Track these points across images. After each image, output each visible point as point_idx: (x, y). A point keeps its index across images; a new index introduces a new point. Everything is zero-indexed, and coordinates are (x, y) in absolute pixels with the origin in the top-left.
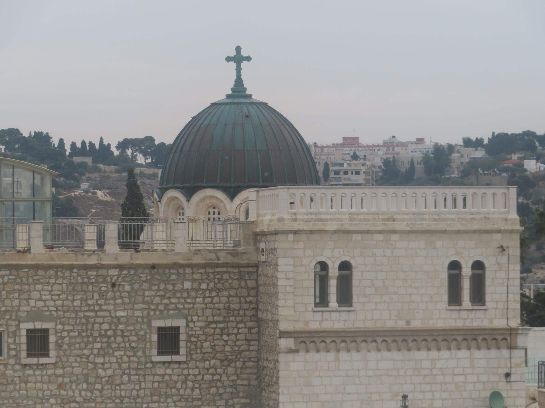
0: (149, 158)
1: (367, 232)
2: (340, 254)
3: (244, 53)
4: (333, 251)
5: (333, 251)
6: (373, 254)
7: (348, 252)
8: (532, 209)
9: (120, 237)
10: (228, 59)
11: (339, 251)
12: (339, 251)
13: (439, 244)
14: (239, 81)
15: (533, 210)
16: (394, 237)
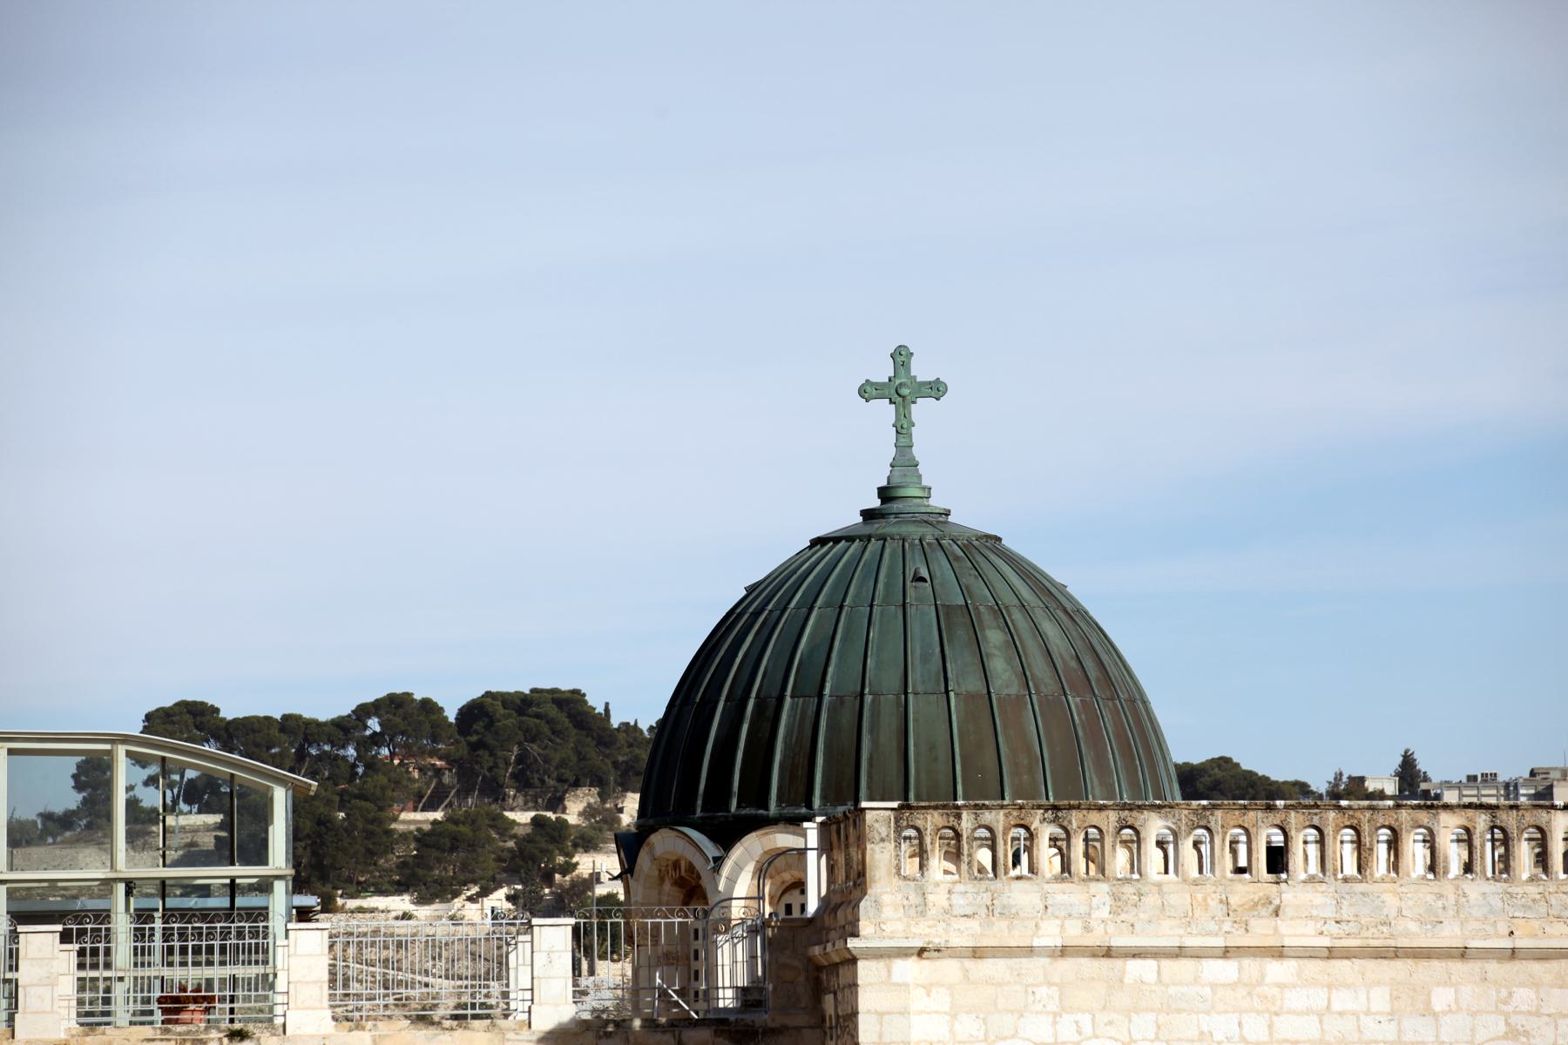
0: (1201, 783)
1: (1179, 953)
2: (1080, 1033)
3: (921, 370)
4: (1055, 1023)
5: (1055, 1023)
6: (1202, 1033)
7: (1110, 1023)
8: (855, 935)
9: (336, 979)
10: (868, 391)
11: (1077, 1022)
12: (1077, 1022)
13: (1442, 998)
14: (904, 460)
15: (991, 645)
16: (1277, 970)
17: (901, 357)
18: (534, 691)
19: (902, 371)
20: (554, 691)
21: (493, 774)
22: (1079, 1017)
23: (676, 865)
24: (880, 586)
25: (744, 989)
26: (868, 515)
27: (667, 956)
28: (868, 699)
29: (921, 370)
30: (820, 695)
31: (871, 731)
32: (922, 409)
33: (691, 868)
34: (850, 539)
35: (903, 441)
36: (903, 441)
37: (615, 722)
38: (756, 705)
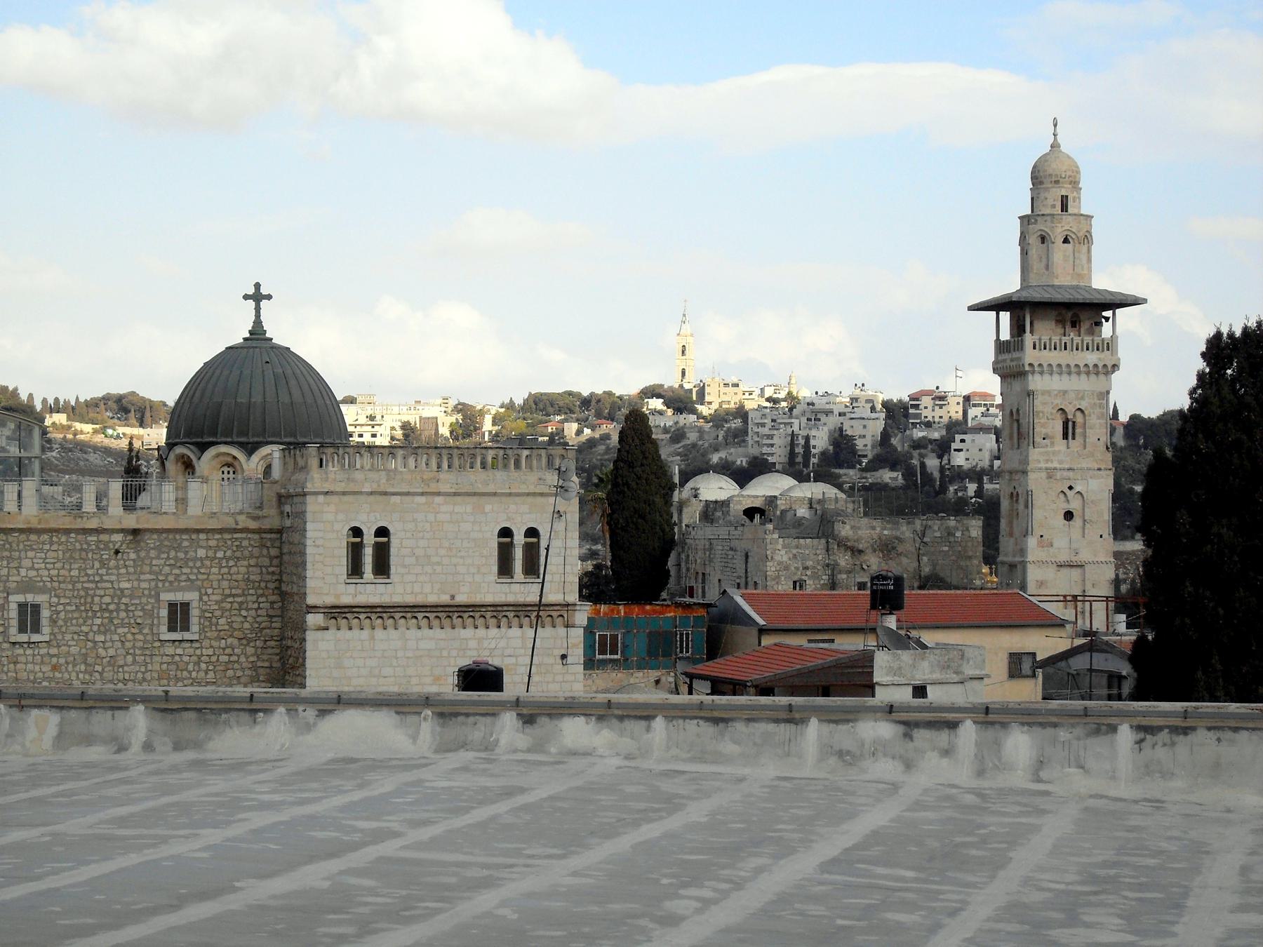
10: (246, 297)
14: (258, 322)
26: (245, 339)
32: (264, 303)
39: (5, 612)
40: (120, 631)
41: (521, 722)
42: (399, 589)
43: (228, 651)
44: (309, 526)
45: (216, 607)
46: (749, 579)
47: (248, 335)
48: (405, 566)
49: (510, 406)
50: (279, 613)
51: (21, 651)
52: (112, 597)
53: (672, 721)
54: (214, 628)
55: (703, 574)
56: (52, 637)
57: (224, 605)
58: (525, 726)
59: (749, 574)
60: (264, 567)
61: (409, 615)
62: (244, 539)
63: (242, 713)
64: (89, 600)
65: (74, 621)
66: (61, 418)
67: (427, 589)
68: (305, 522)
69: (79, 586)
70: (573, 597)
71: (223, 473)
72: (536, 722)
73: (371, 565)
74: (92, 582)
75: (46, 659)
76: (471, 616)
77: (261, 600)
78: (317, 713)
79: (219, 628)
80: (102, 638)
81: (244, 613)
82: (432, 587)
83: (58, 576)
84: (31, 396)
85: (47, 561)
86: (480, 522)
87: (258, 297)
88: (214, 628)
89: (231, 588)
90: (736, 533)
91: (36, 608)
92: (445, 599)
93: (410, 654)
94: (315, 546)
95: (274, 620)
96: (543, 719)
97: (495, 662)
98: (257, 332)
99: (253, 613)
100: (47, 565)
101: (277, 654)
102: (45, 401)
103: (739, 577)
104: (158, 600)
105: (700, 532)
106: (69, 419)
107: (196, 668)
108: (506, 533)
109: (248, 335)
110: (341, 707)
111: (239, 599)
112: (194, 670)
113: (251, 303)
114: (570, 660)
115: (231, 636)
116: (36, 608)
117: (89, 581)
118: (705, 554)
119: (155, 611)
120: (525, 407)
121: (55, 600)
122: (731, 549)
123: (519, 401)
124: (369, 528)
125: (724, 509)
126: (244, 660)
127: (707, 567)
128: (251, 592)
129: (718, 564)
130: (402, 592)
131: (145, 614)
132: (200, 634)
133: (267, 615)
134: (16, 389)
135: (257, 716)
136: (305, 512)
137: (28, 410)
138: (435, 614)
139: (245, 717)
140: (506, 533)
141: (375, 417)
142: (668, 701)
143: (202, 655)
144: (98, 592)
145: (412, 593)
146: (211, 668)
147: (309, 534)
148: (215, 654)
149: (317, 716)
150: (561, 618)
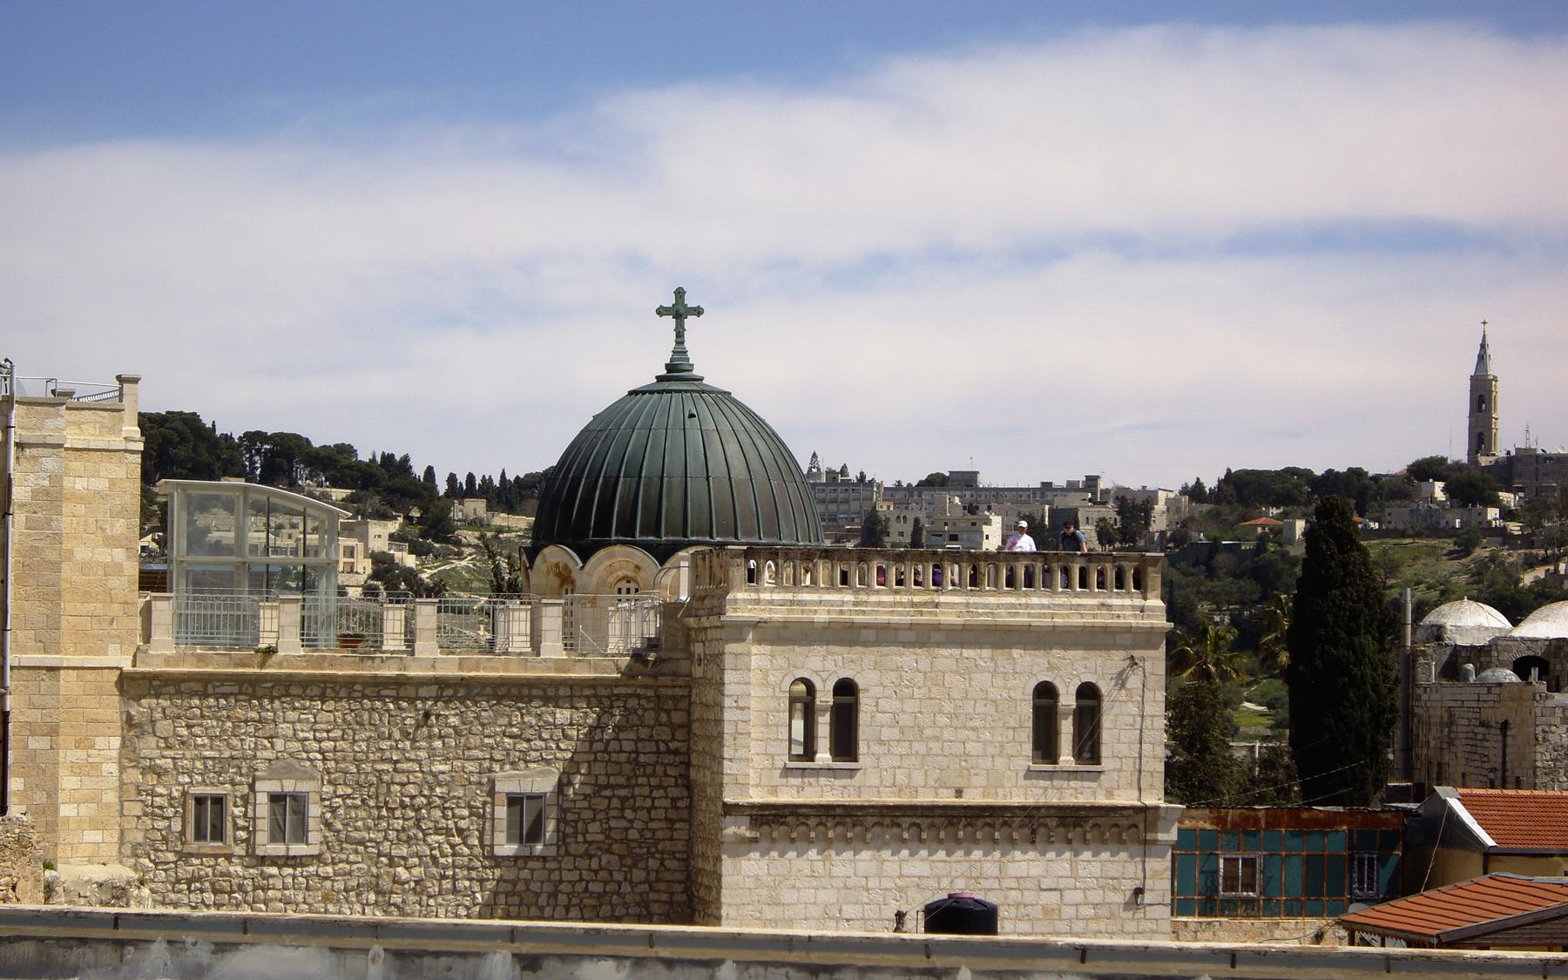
3: (690, 301)
10: (661, 311)
14: (680, 350)
17: (680, 293)
18: (168, 412)
19: (680, 300)
20: (181, 413)
21: (153, 469)
22: (836, 657)
23: (557, 565)
24: (671, 419)
25: (649, 639)
26: (660, 379)
27: (1208, 680)
28: (665, 479)
29: (690, 301)
30: (640, 477)
31: (667, 497)
32: (690, 322)
33: (566, 567)
34: (652, 392)
35: (679, 340)
36: (679, 340)
37: (218, 433)
38: (603, 481)
39: (250, 808)
40: (432, 839)
41: (518, 967)
42: (873, 779)
43: (603, 875)
44: (729, 676)
45: (585, 804)
46: (1508, 774)
47: (664, 372)
48: (880, 742)
49: (1195, 492)
50: (685, 814)
51: (274, 870)
52: (420, 786)
53: (747, 969)
54: (580, 838)
55: (1440, 764)
56: (325, 847)
57: (595, 801)
58: (526, 973)
59: (1509, 766)
60: (663, 741)
61: (888, 821)
62: (631, 696)
63: (102, 947)
64: (383, 789)
65: (360, 824)
66: (477, 507)
67: (918, 779)
68: (722, 670)
69: (366, 767)
70: (1154, 798)
71: (620, 591)
72: (541, 968)
73: (828, 739)
74: (390, 760)
75: (314, 882)
76: (914, 824)
77: (655, 794)
78: (213, 947)
79: (589, 837)
80: (404, 851)
81: (629, 814)
82: (926, 775)
83: (335, 750)
84: (430, 472)
85: (318, 726)
86: (1005, 673)
87: (679, 311)
88: (580, 838)
89: (608, 775)
90: (1491, 697)
91: (299, 800)
92: (946, 798)
93: (888, 884)
94: (737, 708)
95: (677, 825)
96: (552, 962)
97: (991, 899)
98: (677, 370)
99: (643, 814)
100: (318, 734)
101: (680, 882)
102: (452, 479)
103: (1493, 770)
104: (492, 793)
105: (1436, 697)
106: (489, 508)
107: (552, 901)
108: (1045, 692)
109: (664, 372)
110: (249, 937)
111: (623, 792)
112: (548, 905)
113: (670, 322)
114: (1148, 897)
115: (609, 851)
116: (299, 800)
117: (382, 760)
118: (1442, 731)
119: (488, 810)
120: (1219, 495)
121: (328, 789)
122: (1482, 724)
123: (1210, 483)
124: (824, 681)
125: (1483, 659)
126: (629, 889)
127: (1445, 752)
128: (641, 780)
129: (1461, 748)
130: (877, 782)
131: (471, 814)
132: (559, 847)
133: (666, 819)
134: (406, 459)
135: (126, 951)
136: (723, 654)
137: (425, 494)
138: (930, 820)
139: (108, 954)
140: (1045, 692)
141: (977, 508)
142: (1095, 963)
143: (561, 881)
144: (398, 778)
145: (894, 785)
146: (575, 901)
147: (728, 689)
148: (581, 880)
149: (213, 953)
150: (1134, 829)
